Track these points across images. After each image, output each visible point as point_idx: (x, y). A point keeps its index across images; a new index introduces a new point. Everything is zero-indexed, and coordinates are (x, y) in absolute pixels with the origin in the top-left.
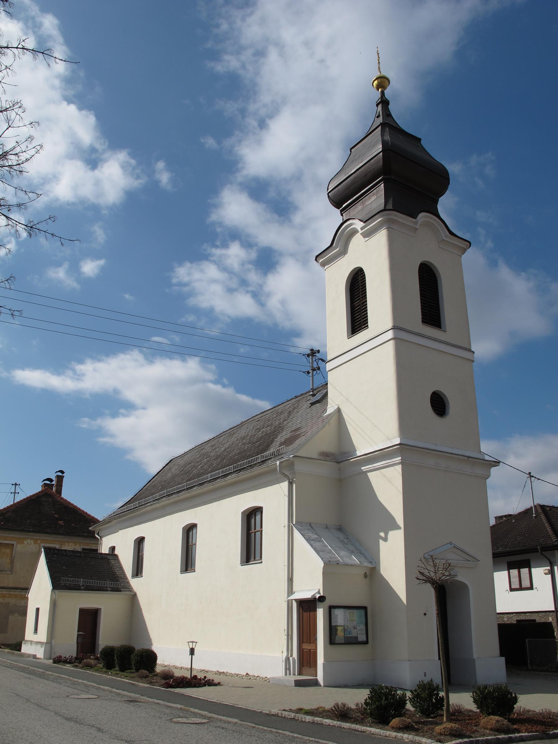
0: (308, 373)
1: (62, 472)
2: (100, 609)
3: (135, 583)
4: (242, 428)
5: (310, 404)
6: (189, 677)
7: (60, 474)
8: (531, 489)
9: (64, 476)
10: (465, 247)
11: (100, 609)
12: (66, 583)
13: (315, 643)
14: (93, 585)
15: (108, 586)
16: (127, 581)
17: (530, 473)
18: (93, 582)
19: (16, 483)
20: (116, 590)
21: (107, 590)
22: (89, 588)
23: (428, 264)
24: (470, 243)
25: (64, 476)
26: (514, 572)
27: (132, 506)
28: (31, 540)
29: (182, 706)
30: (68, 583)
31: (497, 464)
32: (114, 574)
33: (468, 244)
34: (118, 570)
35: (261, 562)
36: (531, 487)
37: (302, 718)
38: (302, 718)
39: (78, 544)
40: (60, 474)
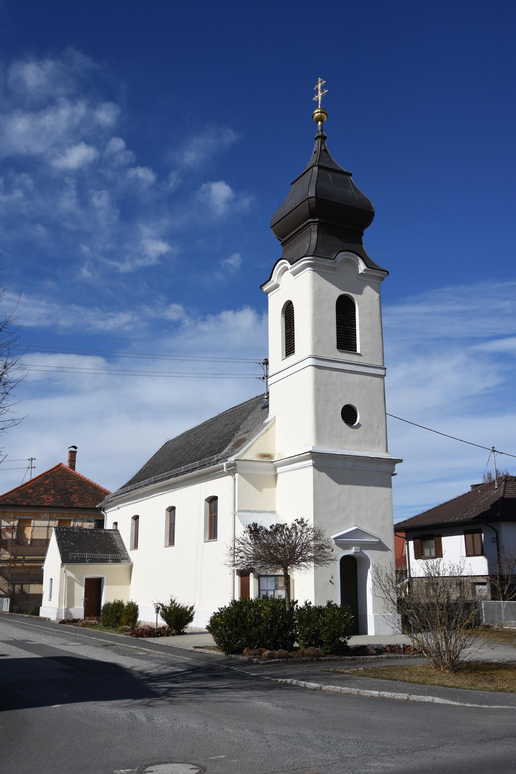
0: (264, 378)
1: (75, 447)
2: (104, 578)
3: (132, 554)
4: (217, 420)
5: (261, 408)
6: (155, 627)
7: (73, 449)
8: (494, 462)
9: (77, 452)
10: (383, 276)
11: (104, 578)
12: (74, 557)
13: (11, 610)
14: (101, 555)
15: (109, 558)
16: (126, 553)
17: (493, 448)
18: (96, 555)
19: (32, 458)
20: (117, 561)
21: (109, 562)
22: (94, 561)
23: (347, 296)
24: (388, 272)
25: (77, 452)
26: (470, 536)
27: (129, 488)
28: (47, 514)
29: (137, 647)
30: (75, 557)
31: (400, 461)
32: (115, 547)
33: (386, 273)
34: (119, 543)
35: (217, 540)
36: (494, 461)
37: (205, 651)
38: (205, 651)
39: (92, 516)
40: (73, 449)
